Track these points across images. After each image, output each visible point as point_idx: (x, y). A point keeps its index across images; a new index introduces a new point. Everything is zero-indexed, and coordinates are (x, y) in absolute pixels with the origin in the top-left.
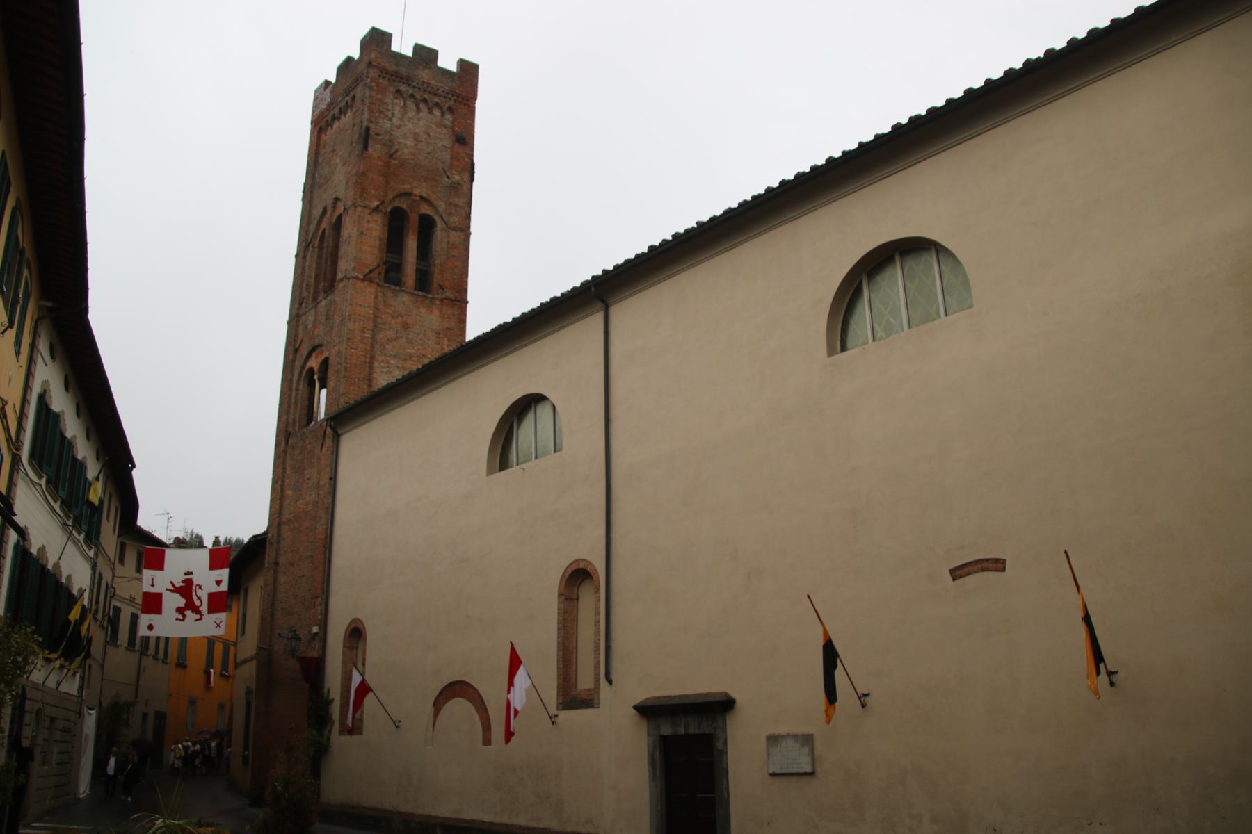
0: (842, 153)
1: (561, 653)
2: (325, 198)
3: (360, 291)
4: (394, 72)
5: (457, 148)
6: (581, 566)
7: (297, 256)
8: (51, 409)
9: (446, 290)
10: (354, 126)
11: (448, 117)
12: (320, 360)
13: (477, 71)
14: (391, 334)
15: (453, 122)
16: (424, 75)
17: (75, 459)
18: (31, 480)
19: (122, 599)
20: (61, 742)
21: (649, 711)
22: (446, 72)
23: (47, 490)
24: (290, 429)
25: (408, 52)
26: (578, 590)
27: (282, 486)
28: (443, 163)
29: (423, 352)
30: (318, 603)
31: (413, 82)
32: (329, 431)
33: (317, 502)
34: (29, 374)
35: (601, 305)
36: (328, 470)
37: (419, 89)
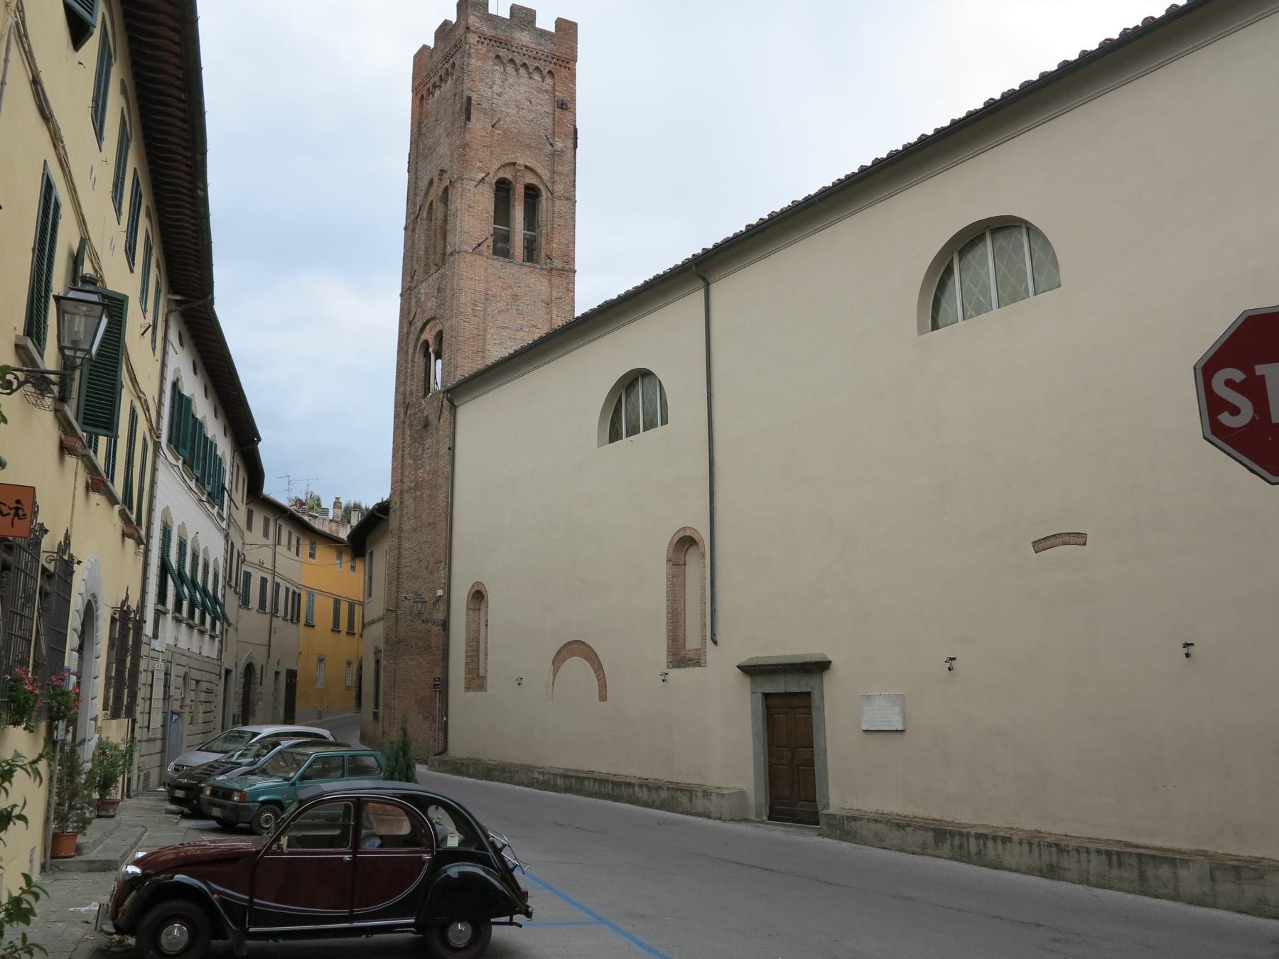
0: (934, 131)
1: (670, 615)
2: (430, 170)
3: (470, 265)
4: (493, 36)
5: (558, 111)
9: (553, 260)
10: (455, 95)
11: (549, 80)
12: (434, 333)
14: (502, 305)
15: (554, 87)
16: (523, 38)
17: (206, 439)
18: (170, 463)
19: (251, 564)
20: (205, 702)
21: (752, 671)
22: (543, 33)
23: (183, 470)
25: (506, 14)
27: (403, 455)
28: (545, 130)
30: (441, 568)
31: (512, 46)
32: (446, 403)
33: (437, 471)
34: (163, 365)
35: (702, 283)
37: (519, 53)
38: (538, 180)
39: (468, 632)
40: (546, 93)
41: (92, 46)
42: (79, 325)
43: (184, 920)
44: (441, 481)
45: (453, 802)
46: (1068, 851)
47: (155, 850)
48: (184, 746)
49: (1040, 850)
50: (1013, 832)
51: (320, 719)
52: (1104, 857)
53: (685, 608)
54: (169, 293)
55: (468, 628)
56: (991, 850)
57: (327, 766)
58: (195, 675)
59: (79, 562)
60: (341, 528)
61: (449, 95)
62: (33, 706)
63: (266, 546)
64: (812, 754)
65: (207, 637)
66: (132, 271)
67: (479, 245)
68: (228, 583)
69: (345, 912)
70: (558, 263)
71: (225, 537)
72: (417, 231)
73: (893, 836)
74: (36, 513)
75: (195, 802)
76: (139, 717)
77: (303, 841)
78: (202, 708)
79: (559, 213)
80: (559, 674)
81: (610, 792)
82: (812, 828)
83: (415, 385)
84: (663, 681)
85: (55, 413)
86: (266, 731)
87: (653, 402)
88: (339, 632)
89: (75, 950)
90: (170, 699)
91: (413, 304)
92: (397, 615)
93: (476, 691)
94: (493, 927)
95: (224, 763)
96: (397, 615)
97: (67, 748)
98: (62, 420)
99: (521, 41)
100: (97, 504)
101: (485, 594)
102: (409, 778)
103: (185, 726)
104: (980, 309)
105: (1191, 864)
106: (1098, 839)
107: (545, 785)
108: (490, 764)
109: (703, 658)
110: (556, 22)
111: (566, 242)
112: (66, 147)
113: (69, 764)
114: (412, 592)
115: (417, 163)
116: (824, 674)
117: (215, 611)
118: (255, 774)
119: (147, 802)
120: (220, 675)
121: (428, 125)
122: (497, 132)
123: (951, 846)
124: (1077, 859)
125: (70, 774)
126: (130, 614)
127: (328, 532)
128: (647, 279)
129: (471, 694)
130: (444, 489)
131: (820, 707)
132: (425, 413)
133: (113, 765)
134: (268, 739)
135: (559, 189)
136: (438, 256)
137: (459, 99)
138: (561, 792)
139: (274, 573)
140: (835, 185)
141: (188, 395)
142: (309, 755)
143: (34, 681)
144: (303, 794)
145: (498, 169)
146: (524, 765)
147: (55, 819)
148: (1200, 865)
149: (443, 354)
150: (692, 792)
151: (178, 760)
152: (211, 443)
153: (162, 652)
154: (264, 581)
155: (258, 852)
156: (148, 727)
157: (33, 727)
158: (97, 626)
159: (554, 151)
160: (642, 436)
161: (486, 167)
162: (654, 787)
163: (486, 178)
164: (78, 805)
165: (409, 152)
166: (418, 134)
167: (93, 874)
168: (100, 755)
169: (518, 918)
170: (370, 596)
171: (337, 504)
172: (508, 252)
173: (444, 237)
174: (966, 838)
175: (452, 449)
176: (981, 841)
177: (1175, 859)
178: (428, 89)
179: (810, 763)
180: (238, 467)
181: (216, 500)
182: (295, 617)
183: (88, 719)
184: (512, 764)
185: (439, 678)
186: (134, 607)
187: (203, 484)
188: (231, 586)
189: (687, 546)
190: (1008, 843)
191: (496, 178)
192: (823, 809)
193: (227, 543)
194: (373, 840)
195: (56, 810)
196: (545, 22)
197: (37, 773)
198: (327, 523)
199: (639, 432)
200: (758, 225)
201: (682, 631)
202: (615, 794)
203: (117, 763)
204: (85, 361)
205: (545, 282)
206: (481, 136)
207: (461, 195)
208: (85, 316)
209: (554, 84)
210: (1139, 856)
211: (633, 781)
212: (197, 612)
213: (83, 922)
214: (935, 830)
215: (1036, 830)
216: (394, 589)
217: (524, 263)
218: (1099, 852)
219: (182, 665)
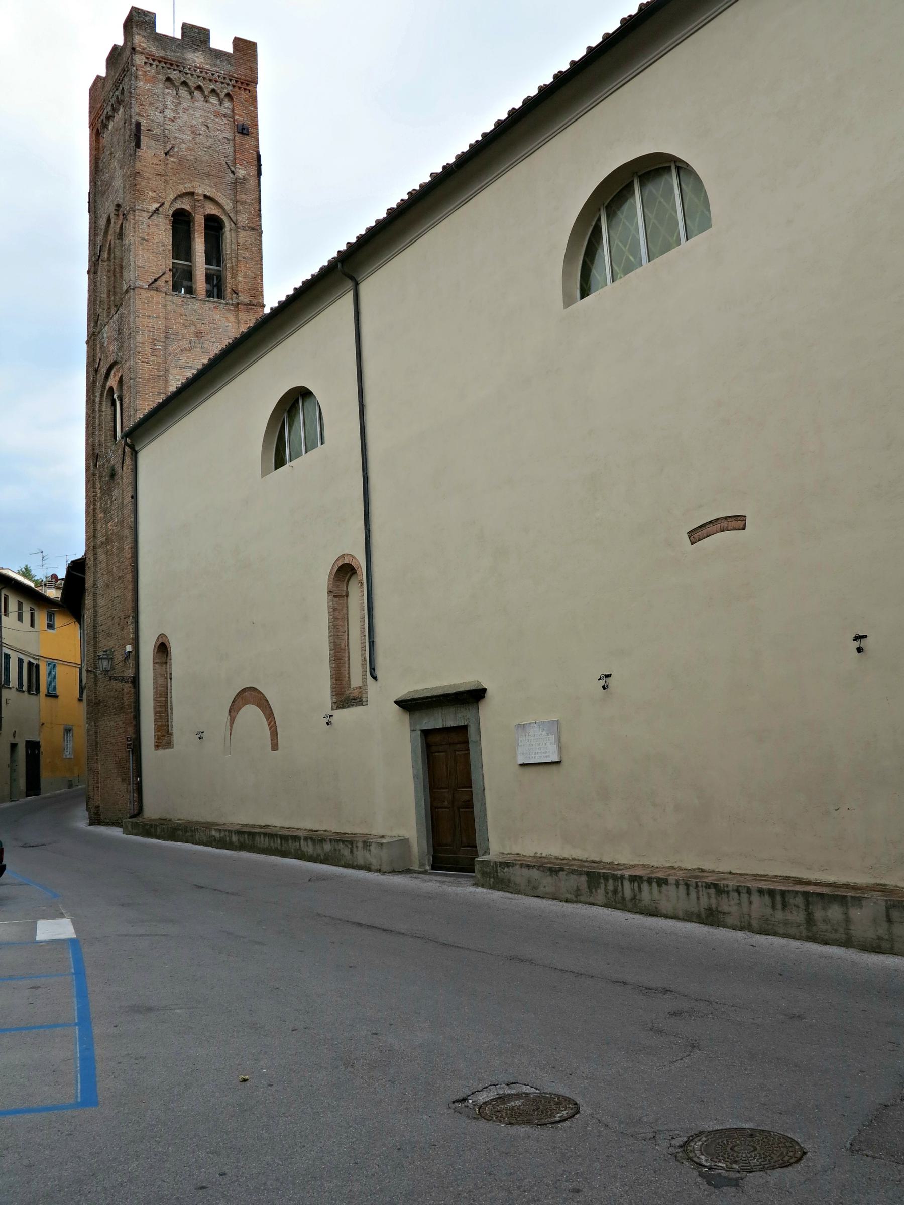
1: (332, 652)
4: (162, 57)
5: (238, 137)
6: (346, 561)
7: (89, 272)
11: (227, 104)
12: (117, 378)
13: (255, 51)
14: (184, 344)
15: (233, 111)
21: (409, 705)
22: (219, 54)
24: (97, 452)
27: (94, 509)
31: (184, 67)
32: (127, 449)
35: (350, 284)
36: (130, 488)
37: (192, 75)
39: (155, 688)
46: (728, 892)
49: (698, 892)
52: (767, 897)
53: (348, 643)
56: (647, 894)
64: (471, 794)
67: (156, 280)
70: (244, 298)
73: (547, 883)
79: (243, 244)
80: (235, 724)
84: (328, 724)
91: (98, 350)
93: (164, 749)
96: (96, 676)
99: (194, 61)
100: (848, 809)
101: (168, 646)
105: (864, 903)
106: (765, 876)
109: (364, 696)
111: (253, 275)
116: (479, 702)
121: (104, 161)
122: (172, 159)
123: (606, 892)
124: (738, 902)
129: (161, 752)
131: (477, 741)
135: (243, 219)
137: (128, 125)
138: (235, 850)
145: (176, 199)
148: (875, 903)
150: (352, 843)
159: (236, 179)
161: (161, 197)
162: (316, 838)
163: (161, 209)
165: (89, 191)
166: (96, 170)
174: (620, 881)
175: (135, 497)
176: (636, 884)
177: (846, 896)
179: (469, 804)
182: (33, 687)
189: (349, 575)
190: (663, 885)
191: (173, 210)
196: (221, 42)
201: (347, 669)
202: (283, 849)
205: (232, 318)
206: (152, 164)
207: (134, 228)
210: (806, 894)
214: (588, 874)
215: (699, 869)
217: (208, 299)
218: (761, 891)
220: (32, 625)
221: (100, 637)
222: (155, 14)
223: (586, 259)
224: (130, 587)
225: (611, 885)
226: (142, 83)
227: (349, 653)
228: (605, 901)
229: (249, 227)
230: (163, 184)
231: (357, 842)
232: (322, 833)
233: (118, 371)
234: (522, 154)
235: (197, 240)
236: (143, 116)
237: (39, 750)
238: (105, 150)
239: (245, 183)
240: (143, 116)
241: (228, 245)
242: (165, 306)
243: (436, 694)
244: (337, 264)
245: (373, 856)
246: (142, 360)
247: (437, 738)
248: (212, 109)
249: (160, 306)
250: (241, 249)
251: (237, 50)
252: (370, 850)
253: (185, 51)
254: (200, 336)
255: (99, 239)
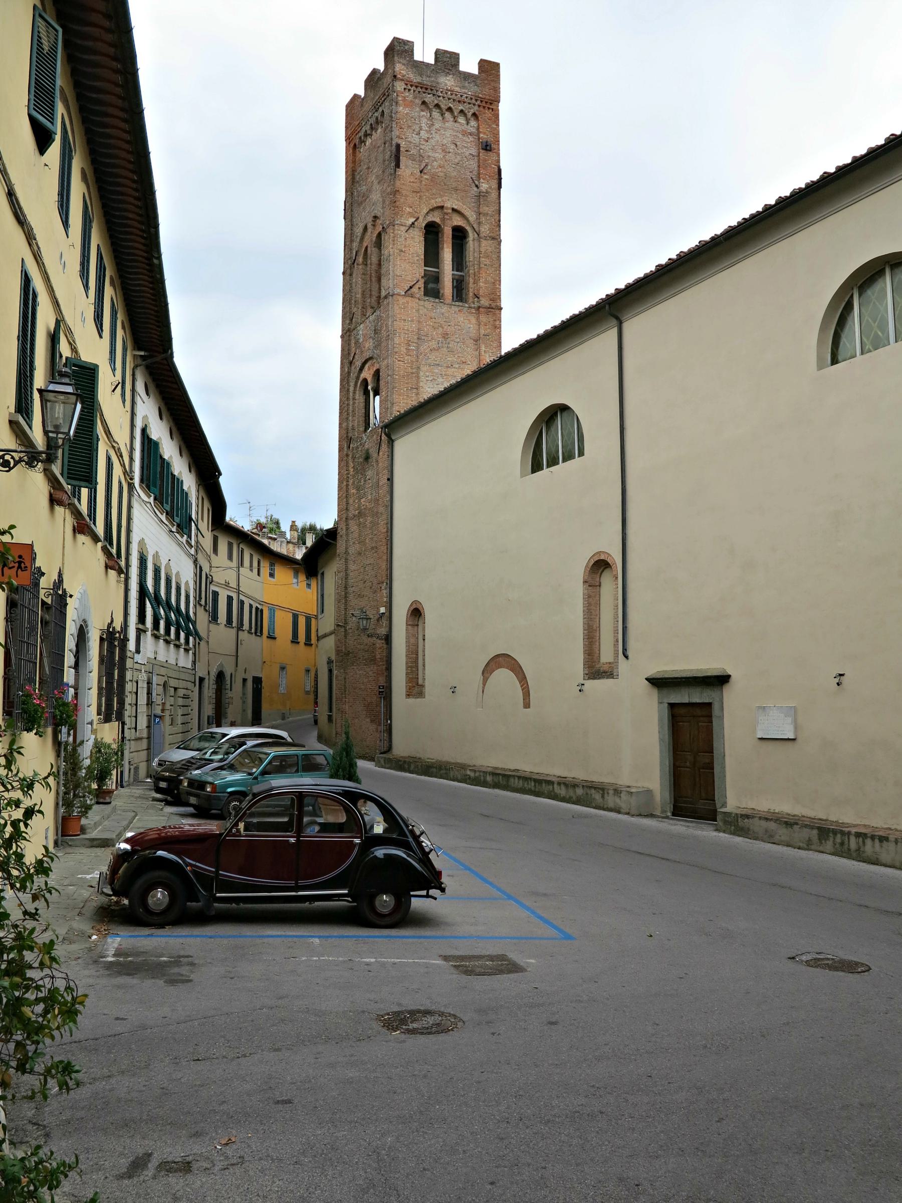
2: (364, 217)
4: (419, 83)
6: (602, 557)
7: (344, 273)
8: (151, 439)
9: (481, 299)
10: (385, 144)
11: (473, 123)
12: (372, 372)
14: (433, 344)
15: (478, 128)
17: (173, 476)
18: (143, 501)
19: (219, 585)
20: (183, 706)
21: (658, 683)
22: (467, 76)
23: (155, 506)
25: (430, 59)
26: (600, 578)
27: (347, 485)
28: (470, 172)
29: (463, 359)
30: (383, 588)
31: (437, 91)
32: (384, 437)
33: (378, 500)
35: (614, 322)
36: (386, 471)
37: (444, 97)
38: (465, 222)
39: (408, 646)
40: (471, 135)
41: (55, 149)
42: (59, 411)
43: (165, 887)
44: (381, 509)
45: (382, 799)
47: (142, 830)
48: (167, 746)
50: (891, 832)
51: (283, 720)
54: (134, 349)
55: (408, 642)
56: (869, 848)
57: (284, 763)
58: (173, 683)
59: (71, 596)
60: (297, 549)
61: (380, 143)
62: (41, 716)
63: (230, 568)
65: (182, 650)
66: (101, 337)
67: (411, 287)
68: (198, 602)
69: (292, 883)
70: (485, 302)
71: (194, 562)
72: (354, 275)
73: (783, 833)
74: (35, 559)
75: (176, 792)
76: (127, 720)
77: (261, 827)
78: (180, 712)
80: (486, 686)
81: (533, 789)
82: (709, 824)
83: (357, 421)
84: (580, 691)
85: (44, 472)
86: (234, 732)
87: (571, 434)
88: (298, 643)
89: (83, 907)
90: (153, 704)
91: (353, 345)
92: (346, 630)
94: (413, 899)
95: (199, 759)
96: (346, 630)
97: (70, 748)
98: (50, 476)
99: (446, 85)
102: (351, 776)
103: (166, 727)
104: (878, 343)
107: (476, 782)
108: (428, 762)
109: (615, 670)
110: (479, 63)
112: (39, 243)
113: (72, 761)
114: (358, 609)
115: (352, 211)
117: (188, 628)
118: (224, 769)
119: (137, 791)
120: (194, 683)
121: (361, 173)
122: (426, 177)
125: (73, 769)
126: (116, 634)
127: (286, 553)
128: (564, 319)
129: (411, 701)
130: (384, 517)
131: (720, 717)
132: (366, 447)
133: (108, 761)
134: (236, 739)
135: (485, 229)
136: (374, 298)
137: (388, 146)
138: (490, 788)
139: (239, 592)
140: (740, 224)
141: (155, 439)
142: (269, 754)
143: (40, 696)
144: (256, 789)
145: (428, 213)
146: (458, 763)
147: (63, 805)
149: (380, 391)
151: (162, 756)
152: (178, 479)
153: (144, 664)
154: (230, 599)
155: (221, 834)
156: (136, 728)
157: (42, 732)
158: (88, 646)
159: (480, 192)
160: (562, 468)
162: (569, 784)
163: (416, 223)
164: (81, 794)
167: (95, 849)
168: (96, 752)
169: (433, 892)
170: (323, 612)
171: (293, 527)
172: (439, 292)
173: (379, 280)
174: (847, 836)
175: (390, 480)
176: (861, 839)
178: (360, 138)
179: (710, 766)
180: (203, 499)
181: (184, 530)
183: (86, 723)
184: (448, 763)
185: (383, 686)
186: (118, 629)
187: (173, 518)
188: (201, 605)
190: (884, 841)
191: (426, 222)
192: (721, 808)
193: (196, 568)
194: (313, 827)
195: (63, 797)
196: (469, 65)
197: (48, 785)
198: (284, 545)
199: (558, 463)
200: (667, 265)
201: (597, 646)
202: (537, 790)
203: (110, 759)
204: (65, 441)
205: (474, 320)
206: (410, 182)
207: (393, 241)
208: (64, 403)
209: (478, 126)
211: (554, 779)
212: (173, 629)
213: (89, 886)
214: (819, 828)
216: (343, 607)
217: (454, 303)
219: (161, 675)
220: (259, 574)
221: (351, 597)
222: (413, 42)
223: (837, 328)
224: (385, 557)
225: (838, 839)
226: (401, 108)
227: (600, 633)
228: (833, 851)
229: (490, 237)
230: (418, 200)
231: (608, 789)
232: (571, 779)
233: (373, 365)
234: (786, 234)
235: (445, 249)
236: (402, 138)
237: (261, 686)
238: (362, 164)
239: (487, 196)
240: (402, 138)
241: (471, 253)
242: (418, 311)
243: (685, 676)
244: (605, 306)
245: (622, 801)
246: (399, 359)
247: (682, 711)
248: (461, 128)
249: (414, 311)
250: (483, 257)
251: (482, 71)
252: (620, 797)
253: (438, 75)
254: (446, 337)
255: (355, 245)
